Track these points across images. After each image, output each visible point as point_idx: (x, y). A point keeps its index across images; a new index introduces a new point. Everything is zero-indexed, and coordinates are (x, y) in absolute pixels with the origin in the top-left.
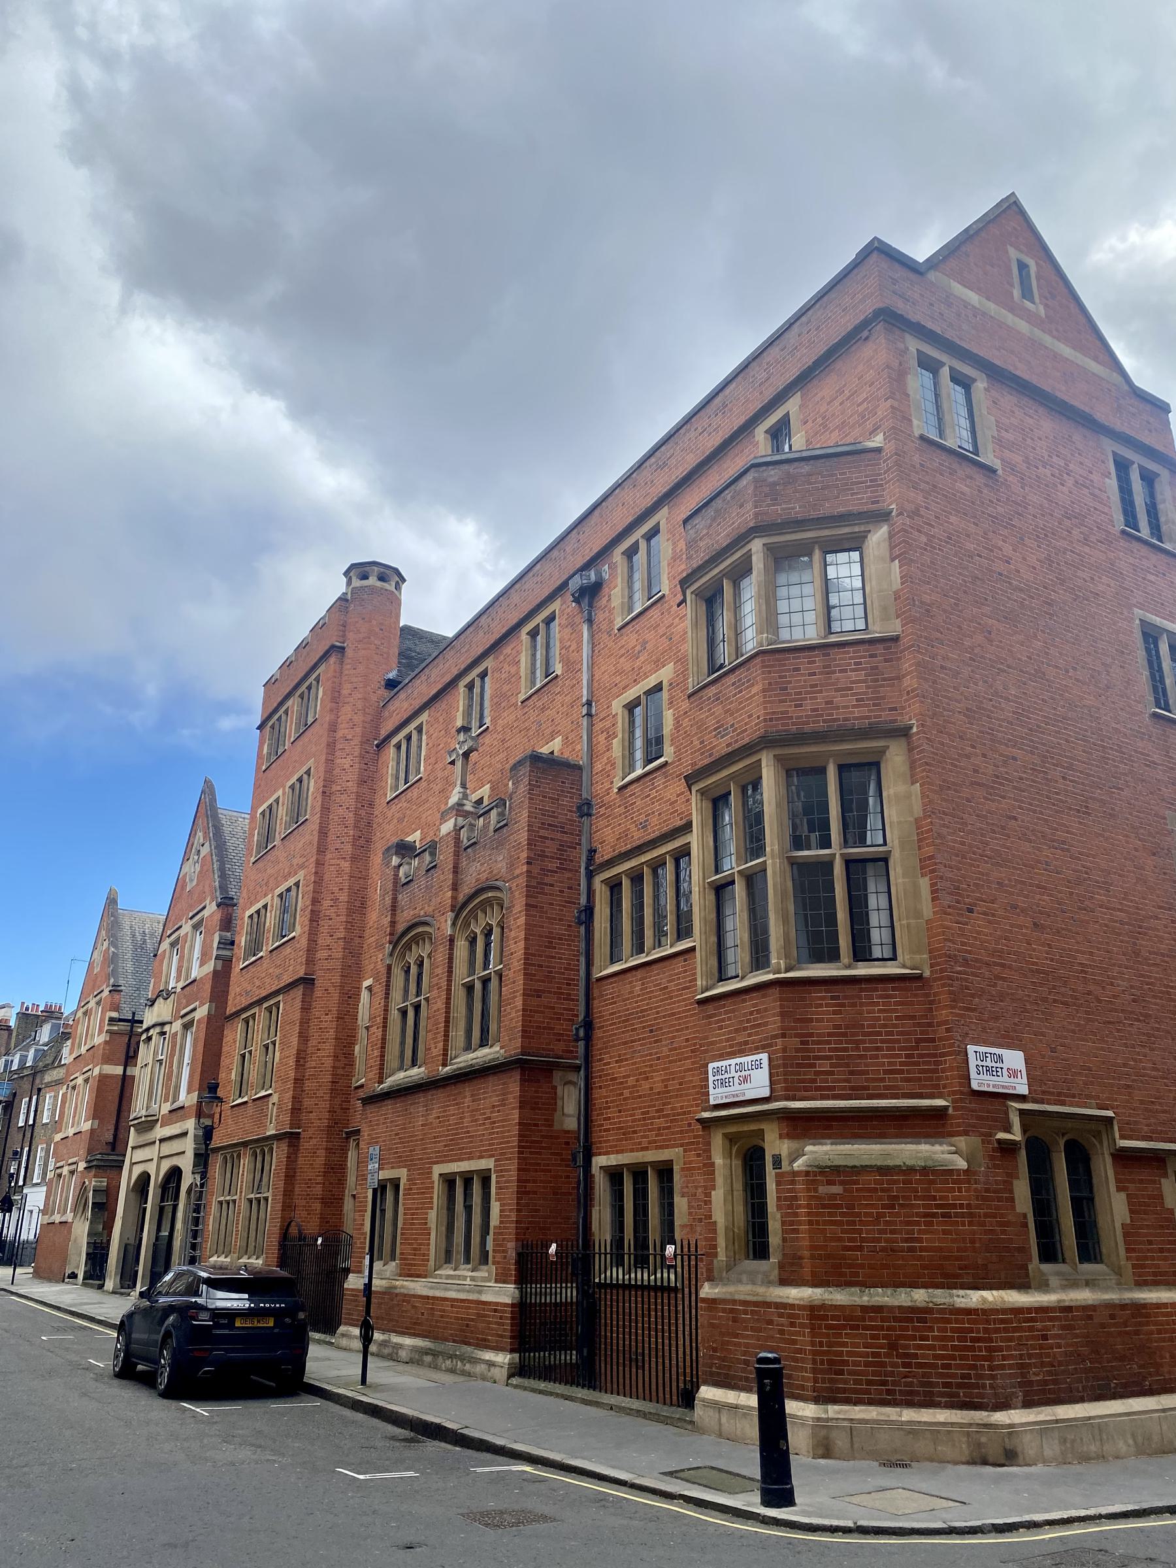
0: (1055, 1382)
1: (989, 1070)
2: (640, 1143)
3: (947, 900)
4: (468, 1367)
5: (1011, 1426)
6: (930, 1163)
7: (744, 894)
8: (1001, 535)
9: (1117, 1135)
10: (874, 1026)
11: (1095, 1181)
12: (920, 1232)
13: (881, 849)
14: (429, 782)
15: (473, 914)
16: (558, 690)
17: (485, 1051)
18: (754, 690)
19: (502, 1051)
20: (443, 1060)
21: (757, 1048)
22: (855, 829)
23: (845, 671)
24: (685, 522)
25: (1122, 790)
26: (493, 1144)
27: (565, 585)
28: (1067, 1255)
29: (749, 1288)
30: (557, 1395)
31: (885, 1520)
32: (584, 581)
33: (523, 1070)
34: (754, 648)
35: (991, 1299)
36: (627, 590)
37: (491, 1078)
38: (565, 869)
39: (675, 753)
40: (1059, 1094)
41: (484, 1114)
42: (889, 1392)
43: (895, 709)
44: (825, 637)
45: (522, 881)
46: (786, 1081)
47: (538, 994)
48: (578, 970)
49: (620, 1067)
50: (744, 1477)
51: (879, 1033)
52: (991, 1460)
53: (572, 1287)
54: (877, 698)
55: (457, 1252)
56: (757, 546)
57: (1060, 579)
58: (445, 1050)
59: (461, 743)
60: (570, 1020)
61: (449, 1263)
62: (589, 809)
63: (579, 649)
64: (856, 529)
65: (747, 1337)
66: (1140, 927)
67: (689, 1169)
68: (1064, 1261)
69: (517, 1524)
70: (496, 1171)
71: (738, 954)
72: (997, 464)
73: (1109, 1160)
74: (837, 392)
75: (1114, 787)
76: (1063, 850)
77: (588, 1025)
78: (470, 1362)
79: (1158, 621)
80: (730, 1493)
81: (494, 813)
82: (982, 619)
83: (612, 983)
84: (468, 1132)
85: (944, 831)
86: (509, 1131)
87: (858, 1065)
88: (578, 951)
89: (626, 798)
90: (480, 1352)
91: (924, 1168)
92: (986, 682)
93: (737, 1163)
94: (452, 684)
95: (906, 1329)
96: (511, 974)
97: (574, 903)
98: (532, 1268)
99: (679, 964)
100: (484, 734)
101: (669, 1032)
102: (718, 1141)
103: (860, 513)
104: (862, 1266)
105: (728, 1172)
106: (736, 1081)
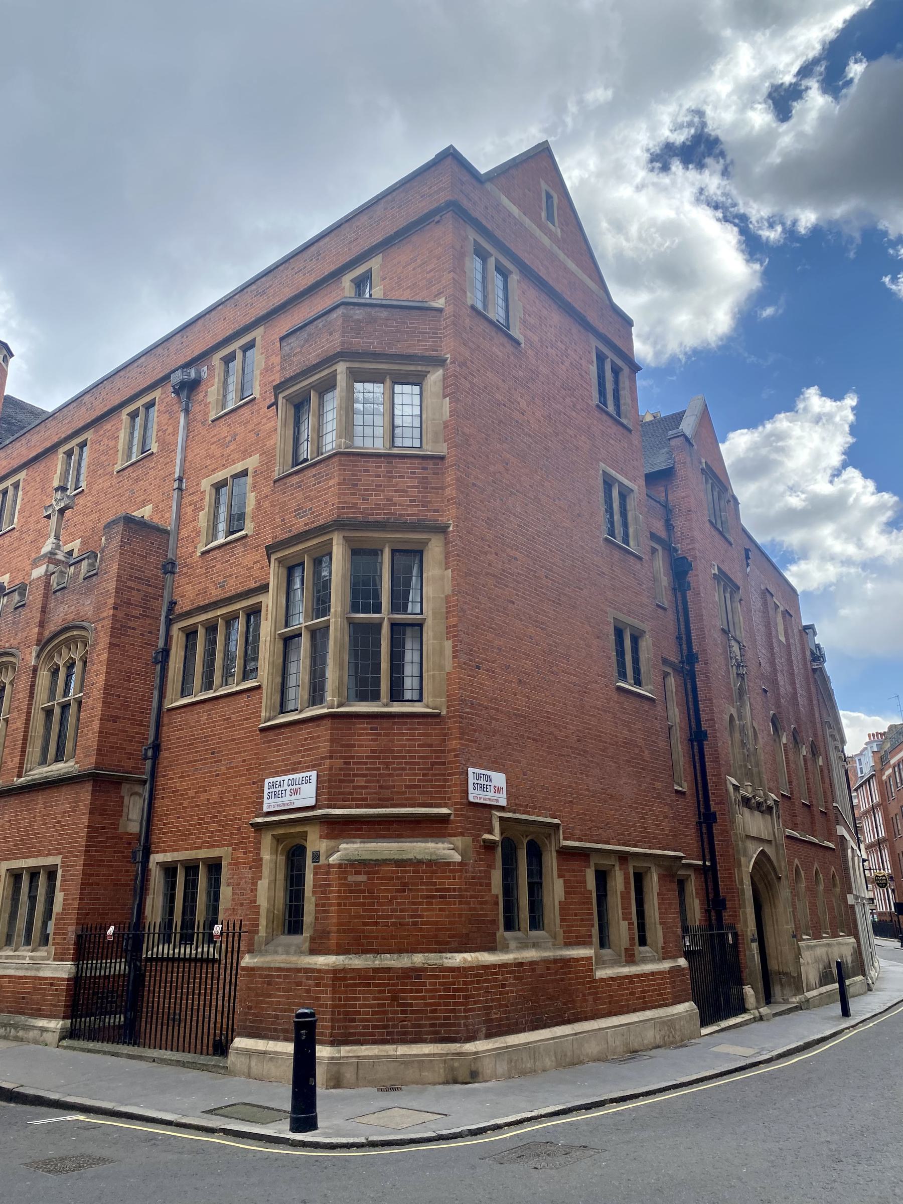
0: (508, 1018)
1: (482, 787)
2: (194, 843)
3: (463, 658)
4: (21, 1034)
5: (476, 1053)
6: (434, 857)
7: (308, 645)
8: (520, 392)
9: (561, 838)
10: (401, 752)
11: (544, 870)
12: (422, 910)
13: (419, 617)
14: (21, 532)
15: (58, 649)
16: (153, 465)
17: (61, 765)
18: (331, 483)
19: (77, 766)
20: (19, 772)
21: (308, 767)
22: (399, 602)
23: (403, 477)
24: (282, 339)
25: (582, 589)
26: (62, 844)
27: (166, 378)
28: (522, 925)
29: (284, 957)
30: (105, 1053)
31: (390, 1134)
32: (186, 377)
33: (95, 781)
34: (333, 449)
35: (469, 959)
36: (222, 389)
37: (64, 789)
38: (147, 616)
39: (255, 528)
40: (526, 806)
41: (55, 818)
42: (388, 1033)
43: (438, 511)
44: (390, 449)
45: (108, 623)
46: (329, 793)
47: (115, 719)
48: (151, 702)
49: (182, 782)
50: (273, 1109)
51: (405, 757)
52: (460, 1079)
53: (120, 962)
54: (426, 501)
55: (19, 936)
56: (341, 368)
57: (555, 433)
58: (21, 763)
59: (58, 501)
60: (140, 742)
61: (10, 945)
62: (173, 568)
63: (175, 433)
64: (419, 368)
65: (279, 997)
66: (586, 688)
67: (235, 864)
68: (519, 930)
69: (80, 1167)
70: (62, 867)
71: (298, 692)
72: (521, 339)
73: (554, 854)
74: (411, 259)
75: (577, 587)
76: (542, 628)
77: (156, 748)
78: (23, 1029)
79: (613, 473)
80: (263, 1124)
81: (85, 564)
82: (502, 453)
83: (180, 713)
84: (38, 833)
85: (466, 607)
86: (78, 833)
87: (386, 781)
88: (153, 685)
89: (207, 561)
90: (34, 1021)
91: (430, 860)
92: (502, 500)
93: (281, 859)
94: (53, 448)
95: (406, 984)
96: (90, 702)
97: (153, 645)
98: (89, 947)
99: (243, 700)
100: (80, 495)
101: (228, 755)
102: (267, 841)
103: (423, 357)
104: (377, 938)
105: (273, 865)
106: (288, 793)
